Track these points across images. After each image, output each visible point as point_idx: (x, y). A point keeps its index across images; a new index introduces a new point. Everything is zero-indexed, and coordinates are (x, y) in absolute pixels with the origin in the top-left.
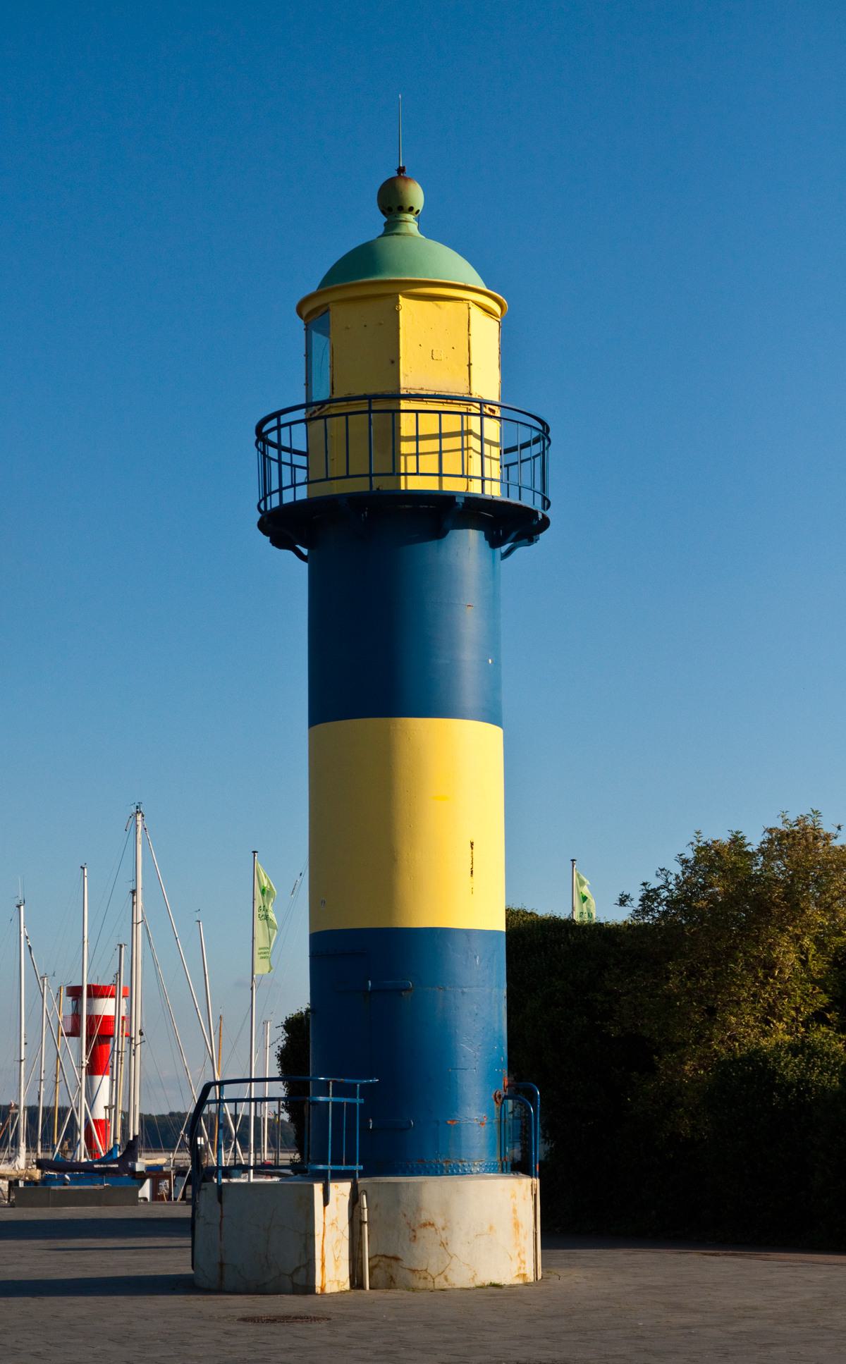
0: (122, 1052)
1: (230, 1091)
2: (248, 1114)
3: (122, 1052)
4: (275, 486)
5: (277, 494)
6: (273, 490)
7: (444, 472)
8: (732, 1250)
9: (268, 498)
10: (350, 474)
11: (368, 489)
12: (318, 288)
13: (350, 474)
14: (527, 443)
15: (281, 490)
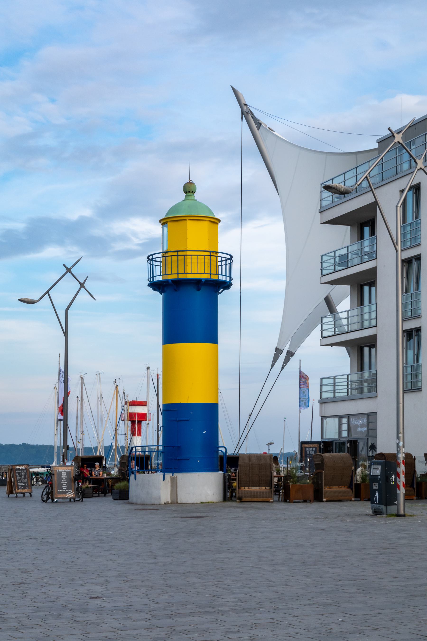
0: (178, 255)
1: (155, 256)
2: (375, 200)
3: (178, 255)
4: (228, 266)
5: (227, 263)
6: (228, 265)
7: (159, 267)
8: (376, 461)
9: (230, 263)
10: (172, 273)
11: (222, 279)
12: (165, 217)
13: (172, 273)
14: (419, 254)
15: (226, 264)
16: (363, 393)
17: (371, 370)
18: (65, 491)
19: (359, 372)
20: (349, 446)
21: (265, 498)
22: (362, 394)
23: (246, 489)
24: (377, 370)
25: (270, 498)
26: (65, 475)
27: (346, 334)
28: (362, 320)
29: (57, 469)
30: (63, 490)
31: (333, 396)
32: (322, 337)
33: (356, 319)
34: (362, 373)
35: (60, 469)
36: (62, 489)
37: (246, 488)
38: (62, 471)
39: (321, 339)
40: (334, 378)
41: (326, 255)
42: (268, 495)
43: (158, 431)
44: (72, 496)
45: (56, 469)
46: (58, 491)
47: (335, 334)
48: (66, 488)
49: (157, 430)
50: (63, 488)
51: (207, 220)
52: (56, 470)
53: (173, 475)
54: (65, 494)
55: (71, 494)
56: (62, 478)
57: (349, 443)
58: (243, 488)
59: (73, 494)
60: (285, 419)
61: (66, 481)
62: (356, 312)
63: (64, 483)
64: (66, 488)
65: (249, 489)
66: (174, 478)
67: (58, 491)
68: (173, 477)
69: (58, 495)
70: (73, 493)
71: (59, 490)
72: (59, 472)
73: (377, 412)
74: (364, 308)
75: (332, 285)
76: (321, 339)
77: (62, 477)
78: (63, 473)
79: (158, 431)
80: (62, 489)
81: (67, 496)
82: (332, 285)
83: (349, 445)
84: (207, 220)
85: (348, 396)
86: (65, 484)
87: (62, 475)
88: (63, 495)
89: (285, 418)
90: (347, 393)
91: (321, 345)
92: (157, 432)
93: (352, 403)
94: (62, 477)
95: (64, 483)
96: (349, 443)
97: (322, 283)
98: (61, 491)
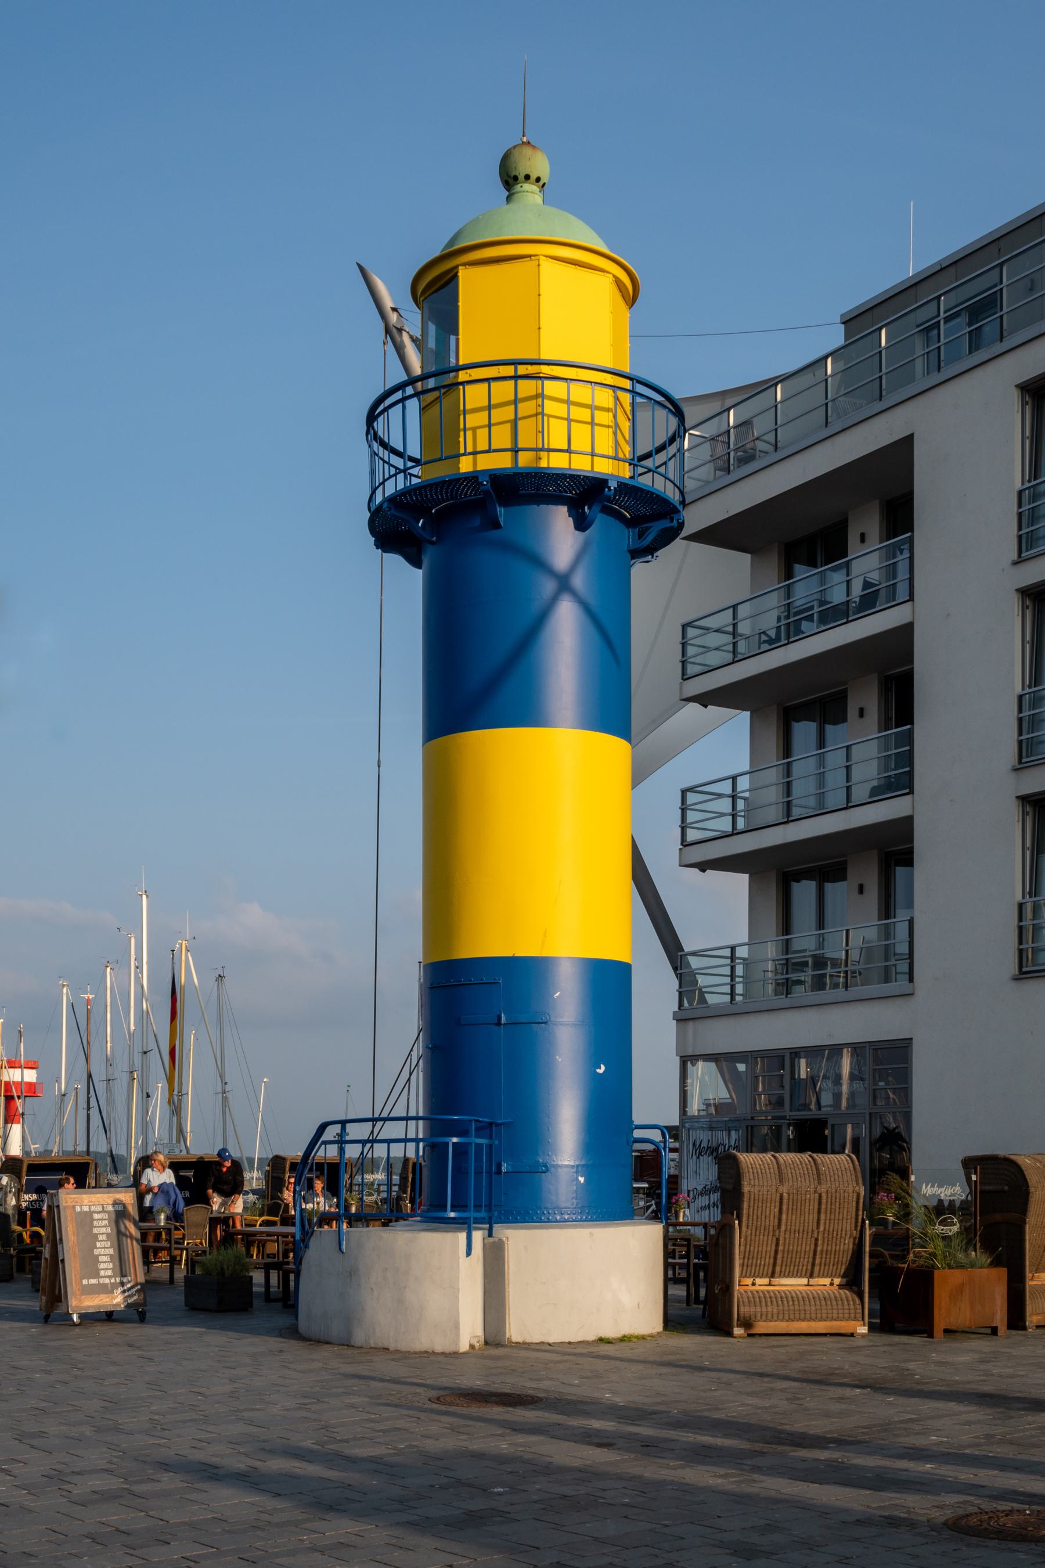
16: (850, 987)
17: (823, 929)
18: (107, 1281)
19: (882, 920)
20: (791, 1137)
21: (836, 1320)
22: (846, 990)
23: (760, 1285)
24: (912, 918)
25: (855, 1319)
26: (106, 1222)
27: (782, 826)
28: (848, 781)
29: (77, 1202)
30: (102, 1281)
31: (729, 1000)
32: (685, 843)
33: (773, 795)
34: (787, 940)
35: (86, 1202)
36: (97, 1275)
37: (759, 1281)
38: (93, 1208)
39: (680, 849)
40: (733, 949)
41: (695, 623)
42: (849, 1309)
43: (89, 1108)
44: (135, 1298)
45: (73, 1204)
46: (85, 1282)
47: (735, 832)
48: (109, 1273)
49: (85, 1106)
50: (102, 1273)
51: (608, 272)
52: (74, 1207)
53: (490, 1235)
54: (111, 1295)
55: (130, 1293)
56: (96, 1235)
57: (791, 1128)
58: (749, 1281)
59: (136, 1291)
60: (348, 1089)
61: (109, 1246)
62: (773, 775)
63: (102, 1251)
64: (109, 1273)
65: (770, 1285)
66: (494, 1242)
67: (85, 1282)
68: (491, 1240)
69: (83, 1297)
70: (136, 1288)
71: (88, 1278)
72: (82, 1213)
73: (912, 1039)
74: (794, 763)
75: (706, 706)
76: (680, 849)
77: (95, 1231)
78: (96, 1216)
79: (89, 1108)
80: (97, 1275)
81: (115, 1302)
82: (706, 706)
83: (792, 1133)
84: (608, 272)
85: (733, 1002)
86: (105, 1255)
87: (95, 1223)
88: (103, 1296)
89: (349, 1086)
90: (729, 996)
91: (680, 866)
92: (85, 1111)
93: (764, 1020)
94: (95, 1231)
95: (102, 1251)
96: (791, 1128)
97: (684, 697)
98: (93, 1281)
